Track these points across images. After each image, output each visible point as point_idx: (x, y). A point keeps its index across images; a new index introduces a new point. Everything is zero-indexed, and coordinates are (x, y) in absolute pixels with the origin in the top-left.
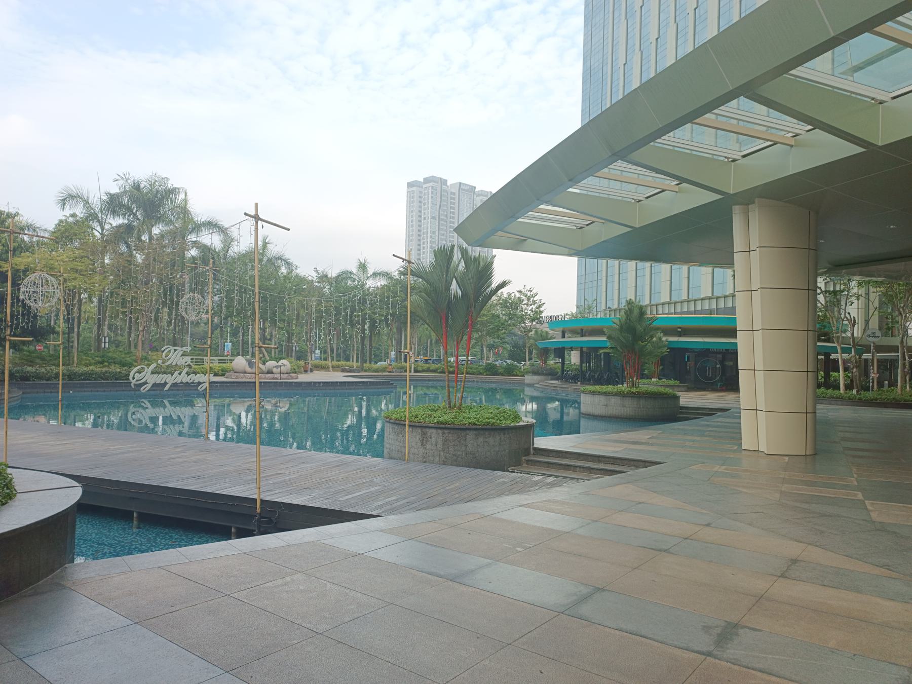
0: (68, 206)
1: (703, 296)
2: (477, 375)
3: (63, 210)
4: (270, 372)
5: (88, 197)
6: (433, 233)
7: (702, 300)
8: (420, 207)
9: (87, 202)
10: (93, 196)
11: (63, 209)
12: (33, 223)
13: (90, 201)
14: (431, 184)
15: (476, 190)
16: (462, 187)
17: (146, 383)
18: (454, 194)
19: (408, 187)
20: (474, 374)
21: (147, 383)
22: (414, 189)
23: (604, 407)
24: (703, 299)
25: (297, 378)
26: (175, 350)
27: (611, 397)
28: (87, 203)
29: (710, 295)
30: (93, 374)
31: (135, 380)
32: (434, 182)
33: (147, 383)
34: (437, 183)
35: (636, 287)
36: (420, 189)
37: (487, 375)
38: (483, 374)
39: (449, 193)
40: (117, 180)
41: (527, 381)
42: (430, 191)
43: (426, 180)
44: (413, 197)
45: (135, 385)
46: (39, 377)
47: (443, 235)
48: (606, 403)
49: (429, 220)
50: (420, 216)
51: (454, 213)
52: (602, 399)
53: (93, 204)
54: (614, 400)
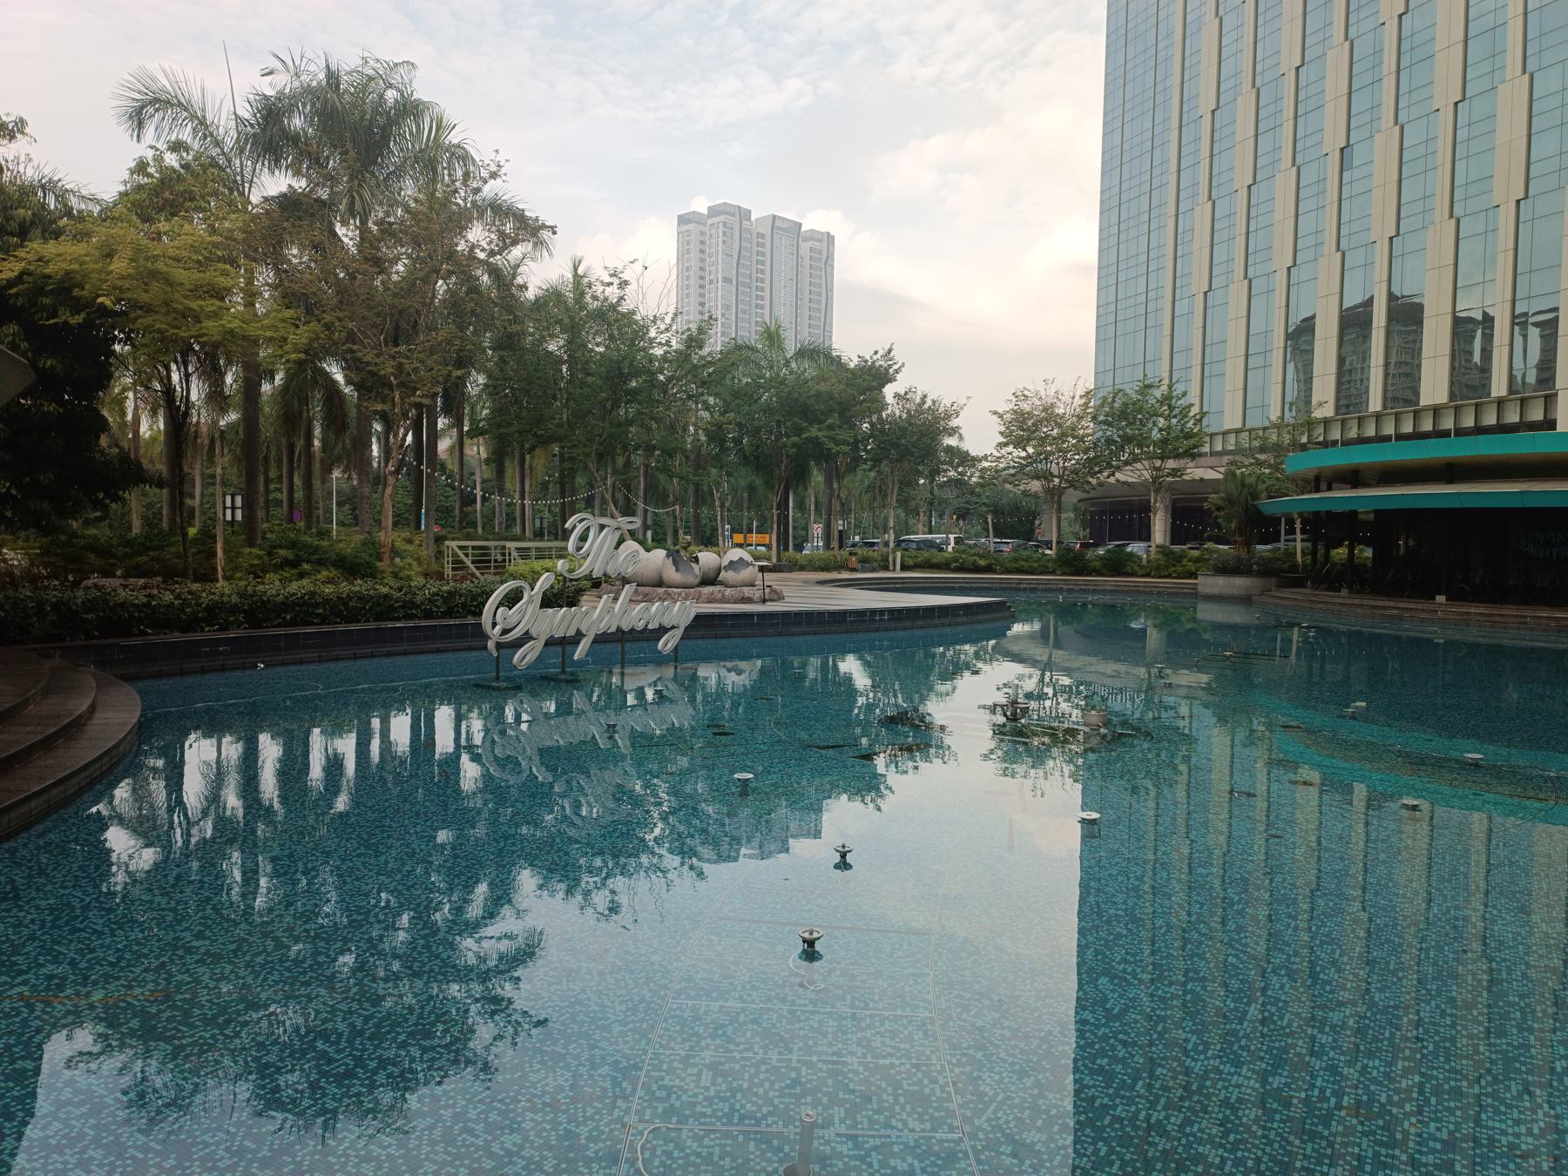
0: (152, 129)
1: (1226, 427)
3: (138, 141)
4: (710, 580)
5: (203, 110)
6: (728, 307)
8: (702, 260)
9: (202, 122)
10: (217, 105)
11: (138, 136)
12: (56, 179)
13: (209, 118)
14: (722, 218)
15: (803, 229)
16: (777, 224)
17: (527, 637)
18: (763, 236)
19: (679, 224)
20: (1032, 573)
21: (532, 638)
22: (691, 226)
24: (1225, 433)
25: (778, 596)
26: (602, 527)
28: (202, 125)
29: (1239, 425)
30: (316, 605)
31: (498, 628)
32: (728, 214)
33: (532, 638)
34: (733, 215)
36: (701, 228)
37: (1064, 574)
38: (1053, 573)
39: (755, 235)
40: (270, 73)
42: (720, 231)
43: (713, 211)
44: (688, 243)
45: (499, 646)
46: (165, 619)
47: (744, 312)
49: (720, 285)
50: (702, 278)
51: (762, 272)
53: (218, 128)
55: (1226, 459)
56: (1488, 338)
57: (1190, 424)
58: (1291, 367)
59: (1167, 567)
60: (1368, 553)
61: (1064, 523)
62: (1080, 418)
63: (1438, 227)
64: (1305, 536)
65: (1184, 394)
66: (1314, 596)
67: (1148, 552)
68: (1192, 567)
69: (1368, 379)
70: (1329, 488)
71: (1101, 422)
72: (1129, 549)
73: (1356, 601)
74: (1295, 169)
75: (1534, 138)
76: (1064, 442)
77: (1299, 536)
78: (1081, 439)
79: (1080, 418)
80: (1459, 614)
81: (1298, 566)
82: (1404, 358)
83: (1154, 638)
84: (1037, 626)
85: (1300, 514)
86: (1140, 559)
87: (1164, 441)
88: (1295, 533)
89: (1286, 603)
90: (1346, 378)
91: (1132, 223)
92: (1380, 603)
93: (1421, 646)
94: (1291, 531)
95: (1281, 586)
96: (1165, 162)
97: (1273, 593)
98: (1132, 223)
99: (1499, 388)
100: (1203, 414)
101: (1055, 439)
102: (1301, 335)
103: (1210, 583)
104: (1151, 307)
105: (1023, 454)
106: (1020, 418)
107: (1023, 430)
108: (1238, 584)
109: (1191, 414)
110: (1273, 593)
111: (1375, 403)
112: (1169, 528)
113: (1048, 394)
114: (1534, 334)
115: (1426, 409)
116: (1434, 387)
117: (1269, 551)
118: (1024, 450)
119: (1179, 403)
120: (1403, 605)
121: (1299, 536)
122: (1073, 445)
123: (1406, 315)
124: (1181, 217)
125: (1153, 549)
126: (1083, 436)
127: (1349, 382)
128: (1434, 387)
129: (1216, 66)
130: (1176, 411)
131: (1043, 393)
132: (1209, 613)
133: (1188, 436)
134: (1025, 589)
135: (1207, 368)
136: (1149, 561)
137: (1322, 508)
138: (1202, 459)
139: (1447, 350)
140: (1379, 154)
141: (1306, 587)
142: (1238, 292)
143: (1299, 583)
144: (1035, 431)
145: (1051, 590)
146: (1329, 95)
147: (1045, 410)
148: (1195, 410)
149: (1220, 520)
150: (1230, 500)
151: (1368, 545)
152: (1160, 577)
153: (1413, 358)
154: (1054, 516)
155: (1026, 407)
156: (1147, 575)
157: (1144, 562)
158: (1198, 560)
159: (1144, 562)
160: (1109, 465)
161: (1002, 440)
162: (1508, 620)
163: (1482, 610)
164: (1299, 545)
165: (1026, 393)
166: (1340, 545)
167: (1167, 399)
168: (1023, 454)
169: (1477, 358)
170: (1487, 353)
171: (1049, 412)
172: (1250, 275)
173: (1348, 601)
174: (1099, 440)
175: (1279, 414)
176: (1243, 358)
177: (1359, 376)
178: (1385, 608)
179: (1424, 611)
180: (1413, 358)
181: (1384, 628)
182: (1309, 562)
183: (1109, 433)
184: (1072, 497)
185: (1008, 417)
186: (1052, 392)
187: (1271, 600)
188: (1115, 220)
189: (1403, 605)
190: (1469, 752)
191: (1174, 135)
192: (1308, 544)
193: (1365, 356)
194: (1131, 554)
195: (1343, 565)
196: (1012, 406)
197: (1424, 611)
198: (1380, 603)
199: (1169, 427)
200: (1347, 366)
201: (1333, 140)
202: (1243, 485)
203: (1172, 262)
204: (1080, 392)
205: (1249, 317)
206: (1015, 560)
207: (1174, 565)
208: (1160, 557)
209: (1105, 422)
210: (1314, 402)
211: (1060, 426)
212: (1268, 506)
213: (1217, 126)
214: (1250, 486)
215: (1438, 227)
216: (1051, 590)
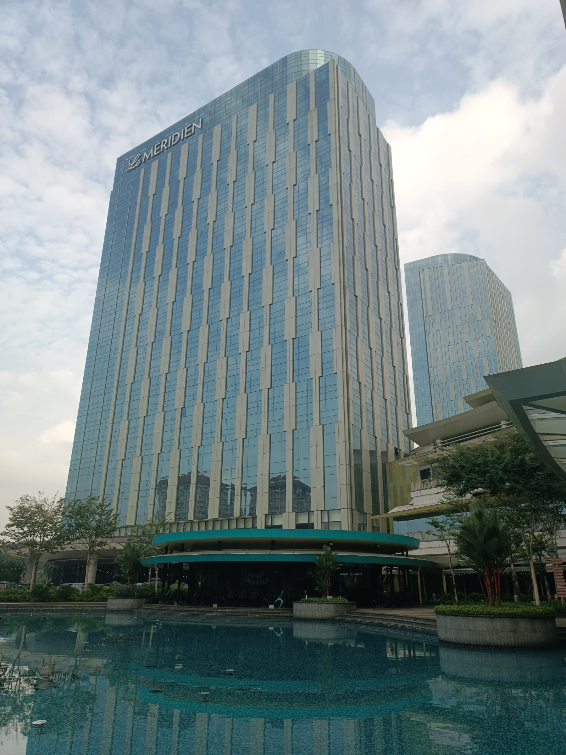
1: (128, 524)
2: (21, 601)
7: (132, 527)
20: (16, 601)
23: (512, 633)
27: (519, 620)
29: (133, 524)
35: (137, 506)
37: (35, 601)
38: (29, 601)
41: (109, 607)
48: (513, 628)
52: (507, 623)
54: (523, 624)
55: (126, 539)
56: (233, 494)
57: (111, 520)
58: (157, 500)
59: (92, 596)
60: (186, 586)
61: (38, 576)
62: (56, 513)
63: (216, 444)
64: (159, 579)
65: (110, 504)
66: (162, 607)
67: (83, 587)
68: (105, 595)
69: (188, 507)
70: (171, 553)
71: (66, 516)
72: (73, 586)
73: (181, 609)
74: (163, 413)
75: (248, 416)
76: (45, 525)
77: (157, 578)
78: (55, 525)
79: (56, 513)
80: (222, 612)
81: (155, 593)
82: (202, 500)
83: (81, 638)
84: (14, 636)
85: (158, 565)
86: (78, 591)
87: (98, 527)
88: (155, 577)
89: (150, 611)
90: (179, 506)
91: (92, 424)
92: (190, 609)
93: (207, 629)
94: (153, 576)
95: (147, 603)
96: (110, 400)
97: (143, 607)
98: (92, 424)
99: (237, 514)
100: (117, 515)
101: (40, 523)
102: (162, 485)
103: (114, 603)
104: (97, 463)
105: (21, 531)
106: (23, 510)
107: (23, 518)
108: (128, 603)
109: (112, 514)
110: (143, 607)
111: (191, 517)
112: (95, 576)
113: (39, 499)
114: (248, 493)
115: (210, 520)
116: (213, 512)
117: (143, 585)
118: (22, 529)
119: (107, 508)
120: (200, 609)
121: (157, 578)
122: (50, 527)
123: (203, 481)
124: (124, 353)
125: (86, 586)
126: (56, 522)
127: (181, 508)
128: (213, 512)
129: (134, 366)
130: (105, 512)
131: (37, 499)
132: (112, 620)
133: (109, 525)
134: (11, 610)
135: (121, 495)
136: (83, 593)
137: (168, 561)
138: (115, 539)
139: (218, 496)
140: (197, 411)
141: (158, 603)
142: (137, 461)
143: (155, 601)
144: (30, 519)
145: (27, 611)
146: (178, 387)
147: (37, 507)
148: (114, 512)
149: (121, 568)
150: (127, 558)
151: (186, 583)
152: (87, 602)
153: (205, 500)
154: (34, 567)
155: (27, 505)
156: (81, 601)
157: (80, 593)
158: (108, 591)
159: (80, 593)
160: (68, 539)
161: (10, 522)
162: (241, 614)
163: (231, 610)
164: (157, 582)
165: (28, 498)
166: (174, 582)
167: (101, 506)
168: (21, 531)
169: (229, 502)
170: (232, 500)
171: (39, 510)
172: (143, 454)
173: (177, 609)
174: (64, 525)
175: (151, 517)
176: (137, 492)
177: (184, 506)
178: (192, 611)
179: (208, 612)
180: (205, 500)
181: (191, 622)
182: (160, 591)
183: (70, 522)
184: (45, 556)
185: (16, 510)
186: (42, 498)
187: (142, 610)
188: (84, 421)
189: (200, 609)
190: (228, 669)
191: (112, 408)
192: (161, 582)
193: (187, 497)
194: (74, 589)
195: (176, 590)
196: (19, 504)
197: (208, 612)
198: (190, 609)
199: (101, 520)
200: (179, 502)
201: (179, 404)
202: (134, 550)
203: (109, 444)
204: (58, 499)
205: (141, 473)
206: (7, 593)
207: (96, 594)
208: (89, 590)
209: (69, 516)
210: (167, 512)
211: (44, 516)
212: (145, 561)
213: (133, 390)
214: (137, 551)
215: (216, 444)
216: (27, 611)
